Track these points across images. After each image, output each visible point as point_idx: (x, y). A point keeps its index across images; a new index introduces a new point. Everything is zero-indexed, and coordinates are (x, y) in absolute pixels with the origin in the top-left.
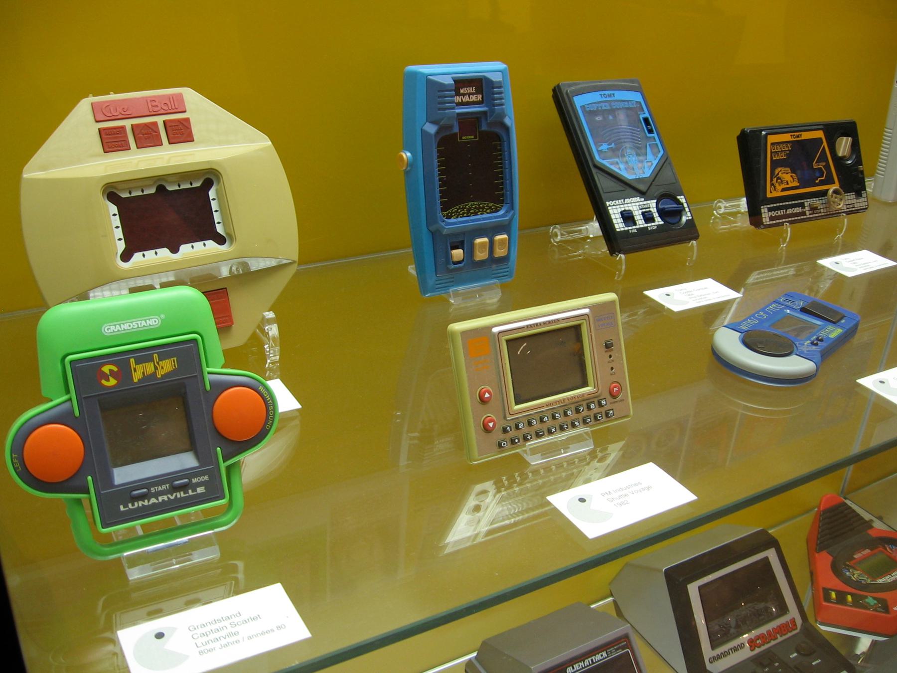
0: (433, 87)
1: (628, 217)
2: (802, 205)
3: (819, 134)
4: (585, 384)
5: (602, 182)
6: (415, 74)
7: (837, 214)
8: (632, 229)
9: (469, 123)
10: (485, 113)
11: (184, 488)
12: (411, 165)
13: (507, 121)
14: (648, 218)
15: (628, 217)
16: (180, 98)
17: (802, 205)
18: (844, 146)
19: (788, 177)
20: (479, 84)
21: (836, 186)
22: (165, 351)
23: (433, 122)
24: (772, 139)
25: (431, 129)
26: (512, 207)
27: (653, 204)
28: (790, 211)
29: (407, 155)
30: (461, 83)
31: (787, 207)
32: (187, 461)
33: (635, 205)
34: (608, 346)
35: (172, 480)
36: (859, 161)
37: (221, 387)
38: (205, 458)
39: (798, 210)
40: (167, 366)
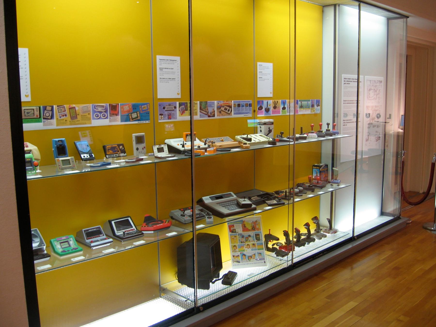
0: (56, 141)
1: (84, 157)
2: (114, 155)
3: (116, 145)
4: (70, 165)
5: (80, 153)
6: (53, 140)
7: (121, 157)
8: (85, 158)
9: (60, 145)
10: (62, 144)
11: (31, 169)
12: (54, 150)
13: (66, 145)
14: (87, 156)
15: (84, 157)
16: (27, 143)
17: (114, 155)
18: (121, 147)
19: (111, 151)
20: (61, 141)
21: (120, 152)
22: (30, 158)
23: (56, 145)
24: (107, 147)
25: (56, 146)
26: (67, 155)
27: (88, 155)
28: (111, 156)
29: (53, 149)
30: (59, 141)
31: (111, 155)
32: (32, 167)
33: (86, 155)
34: (73, 162)
35: (31, 169)
36: (124, 149)
37: (34, 162)
38: (33, 167)
39: (113, 156)
40: (30, 159)
